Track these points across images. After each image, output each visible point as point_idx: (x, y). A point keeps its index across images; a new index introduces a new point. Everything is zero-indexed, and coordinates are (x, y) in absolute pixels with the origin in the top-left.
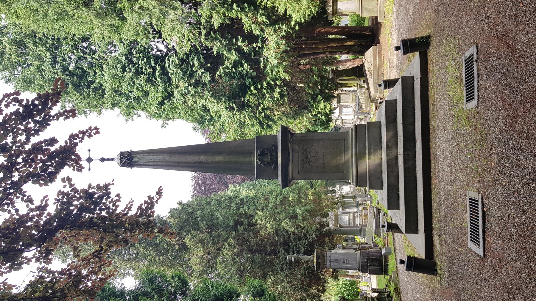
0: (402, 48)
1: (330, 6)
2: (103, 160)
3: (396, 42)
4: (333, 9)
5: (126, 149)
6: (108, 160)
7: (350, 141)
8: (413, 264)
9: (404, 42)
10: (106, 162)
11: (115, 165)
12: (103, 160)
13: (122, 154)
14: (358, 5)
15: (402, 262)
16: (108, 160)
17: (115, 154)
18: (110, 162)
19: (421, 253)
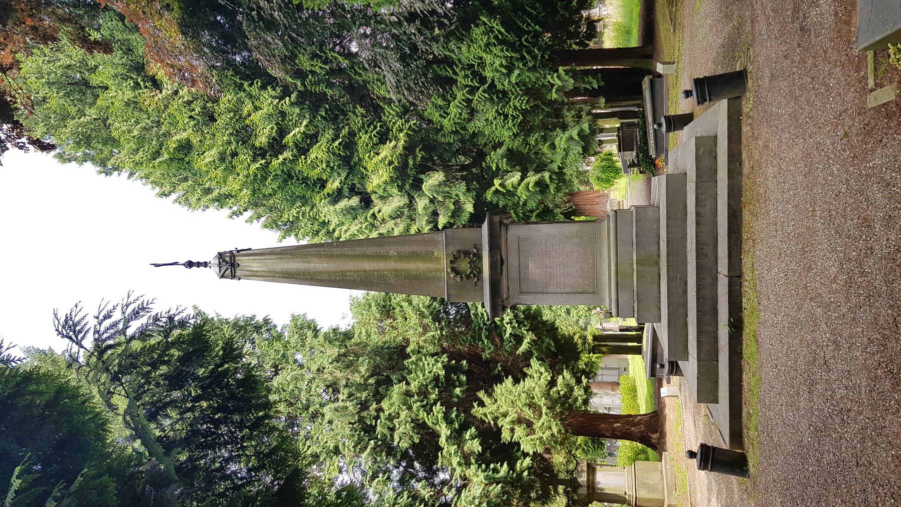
0: (699, 456)
1: (582, 471)
2: (190, 264)
3: (687, 84)
4: (588, 479)
5: (228, 247)
6: (199, 264)
7: (606, 253)
8: (709, 458)
9: (703, 447)
10: (194, 268)
11: (212, 273)
12: (190, 264)
13: (221, 255)
14: (630, 480)
15: (692, 454)
16: (199, 264)
17: (210, 256)
18: (202, 268)
19: (723, 442)
